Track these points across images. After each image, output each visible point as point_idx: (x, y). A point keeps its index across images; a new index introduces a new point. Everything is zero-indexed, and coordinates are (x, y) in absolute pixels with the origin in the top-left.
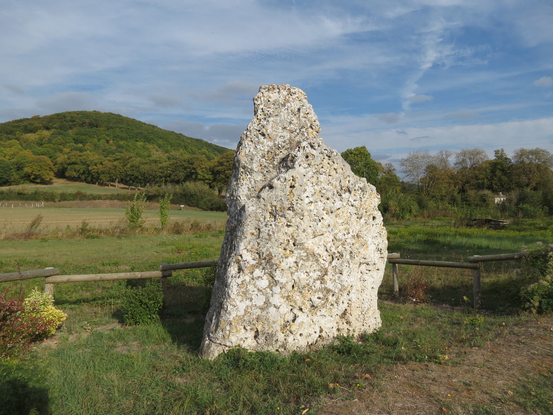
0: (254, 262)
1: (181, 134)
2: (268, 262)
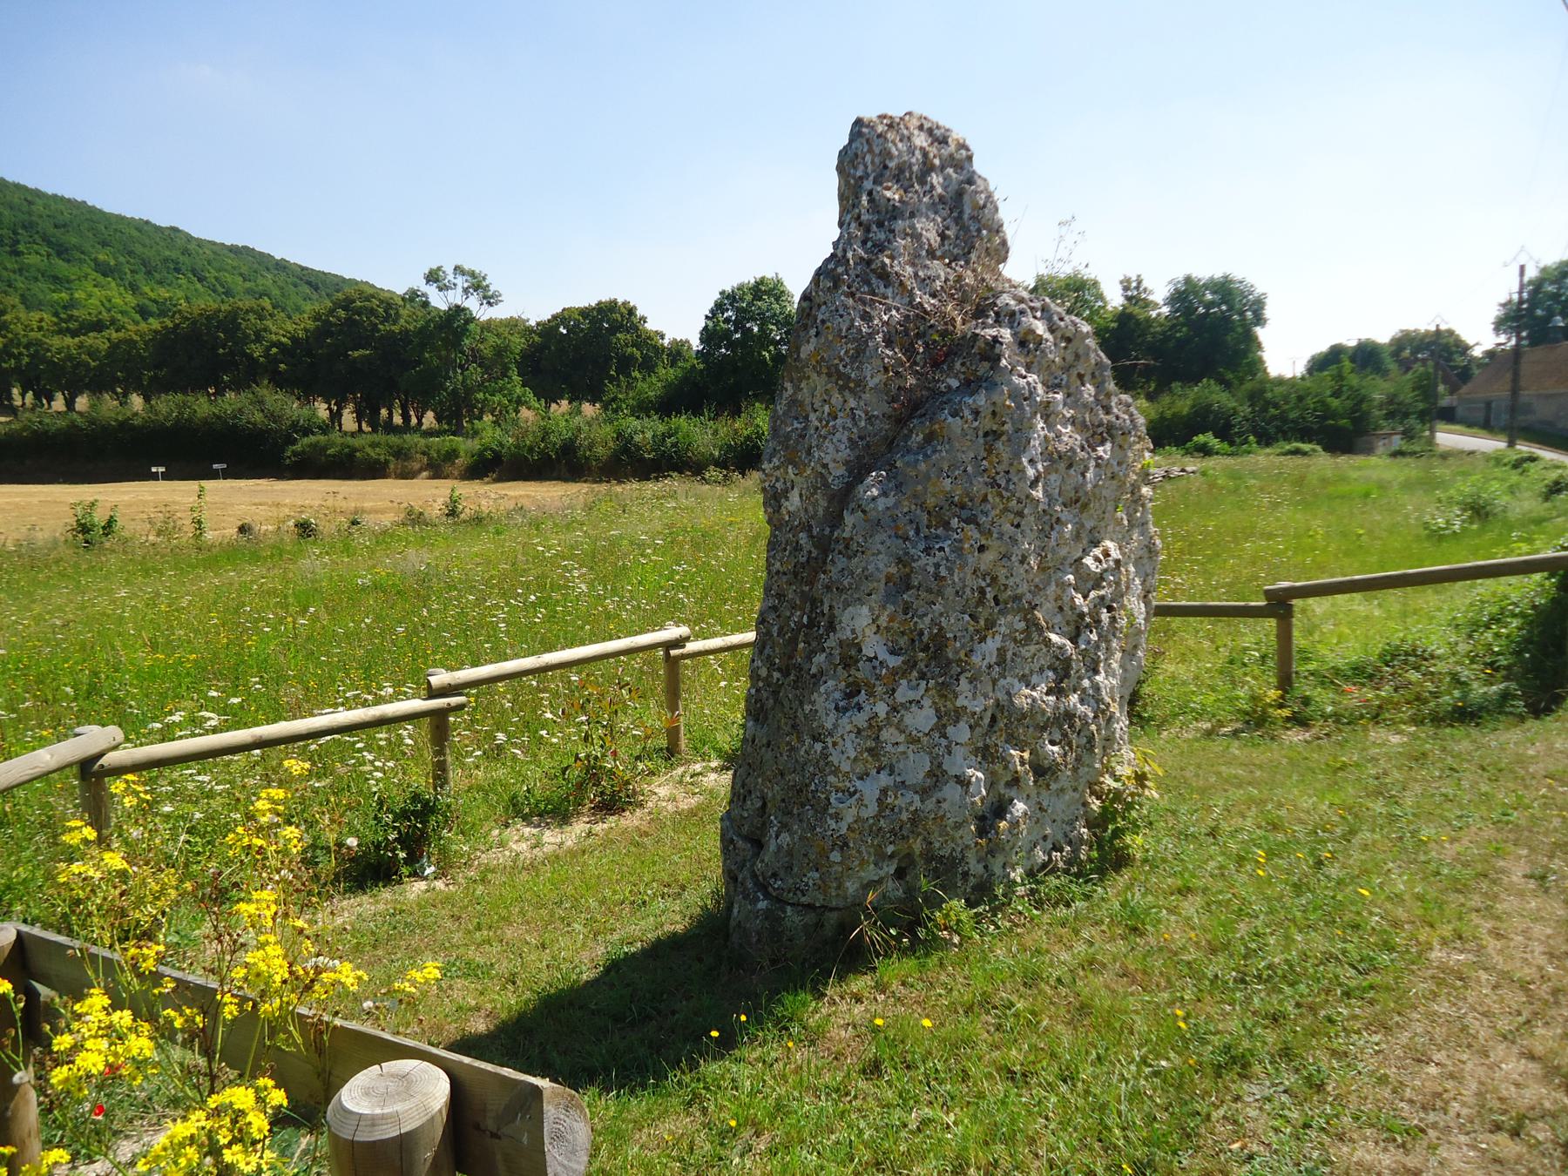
0: (894, 662)
1: (175, 230)
2: (934, 657)
